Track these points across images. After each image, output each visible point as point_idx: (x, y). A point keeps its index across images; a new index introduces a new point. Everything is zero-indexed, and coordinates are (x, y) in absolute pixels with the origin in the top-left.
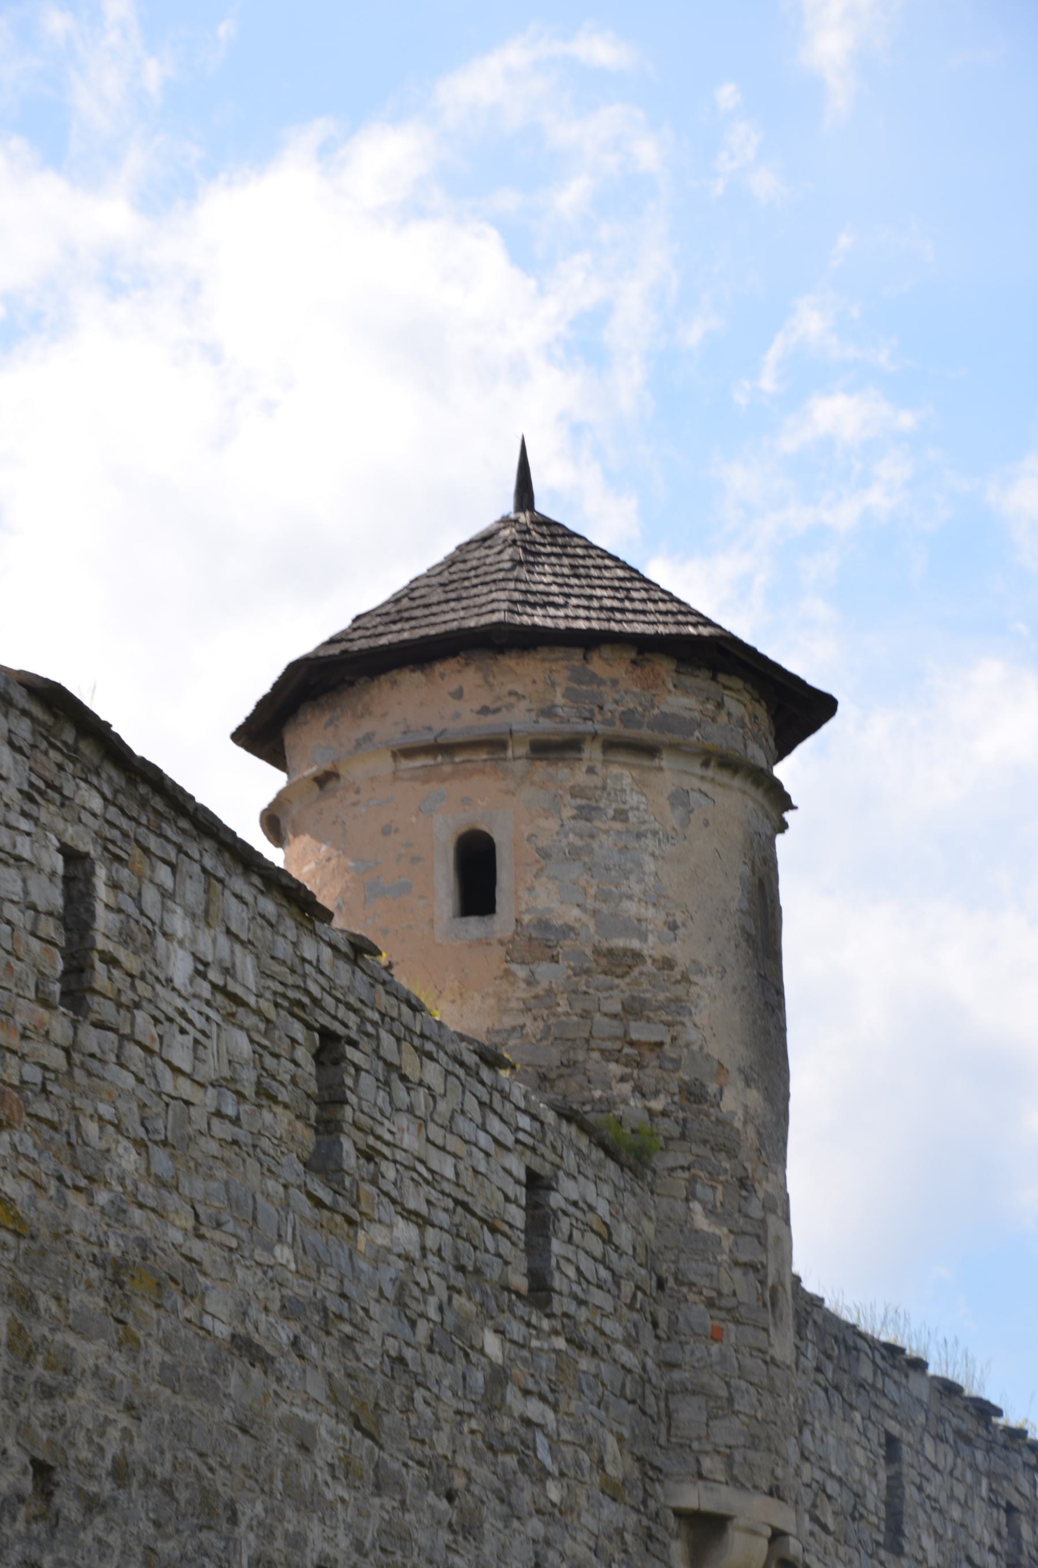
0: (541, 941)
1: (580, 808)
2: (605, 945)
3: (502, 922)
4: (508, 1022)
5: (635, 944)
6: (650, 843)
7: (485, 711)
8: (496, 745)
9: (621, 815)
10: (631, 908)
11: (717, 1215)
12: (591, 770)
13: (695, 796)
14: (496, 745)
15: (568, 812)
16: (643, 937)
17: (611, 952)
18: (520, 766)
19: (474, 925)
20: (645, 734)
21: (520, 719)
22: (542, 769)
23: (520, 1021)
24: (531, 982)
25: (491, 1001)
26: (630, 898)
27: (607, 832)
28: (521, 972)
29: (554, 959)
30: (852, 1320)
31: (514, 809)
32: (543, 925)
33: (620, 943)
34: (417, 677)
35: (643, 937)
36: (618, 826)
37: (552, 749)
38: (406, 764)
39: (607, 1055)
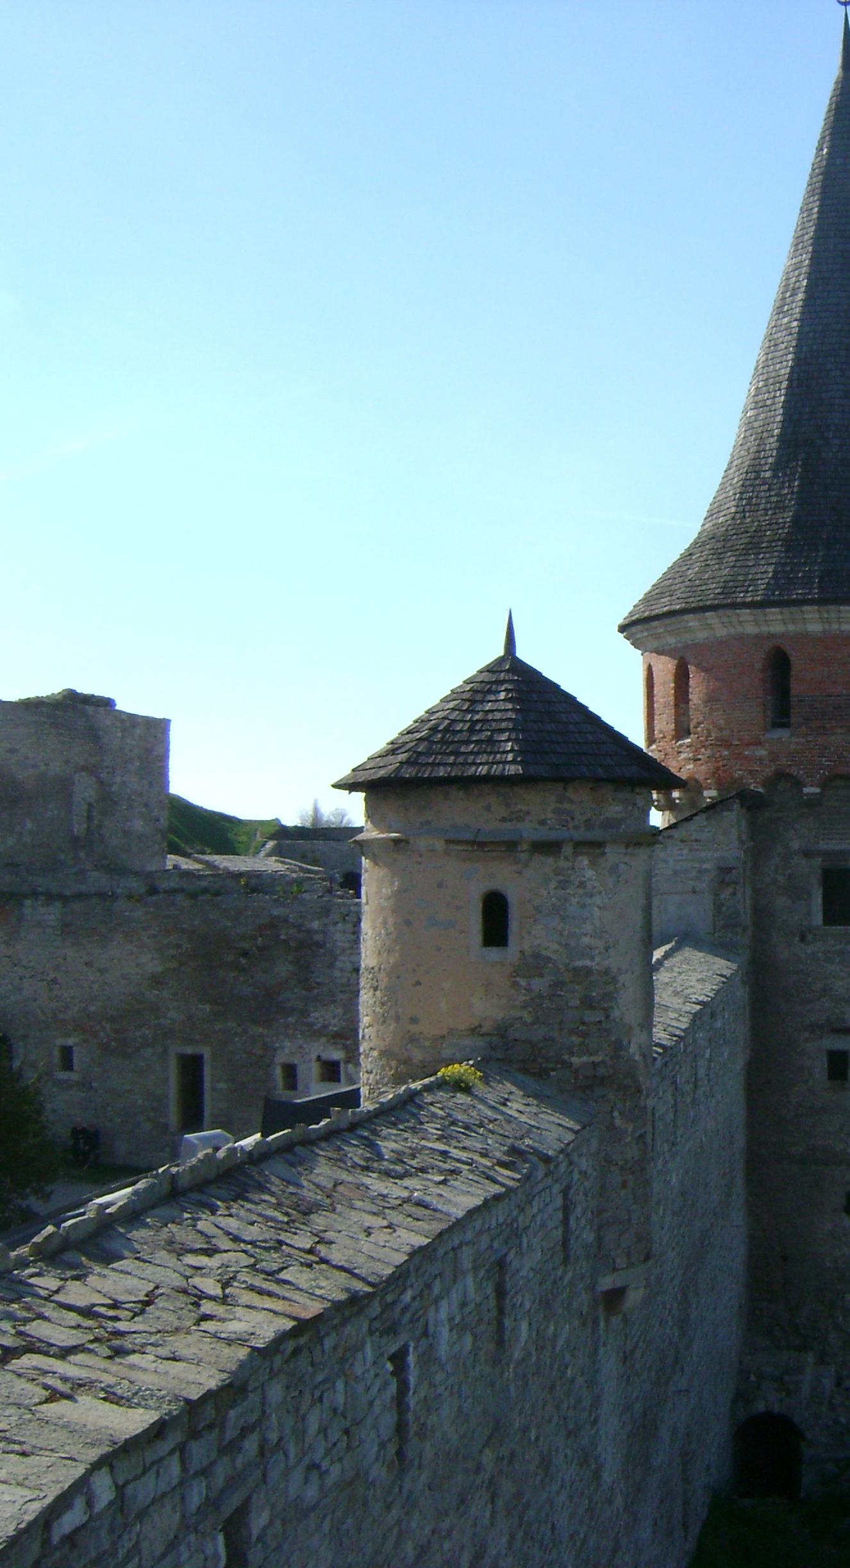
0: (534, 964)
1: (560, 882)
2: (573, 964)
3: (511, 953)
4: (515, 1013)
5: (588, 963)
6: (597, 900)
7: (504, 820)
8: (511, 846)
9: (582, 885)
10: (586, 940)
11: (405, 1103)
12: (566, 859)
13: (622, 866)
14: (511, 846)
15: (553, 885)
16: (592, 958)
17: (574, 969)
18: (523, 856)
19: (494, 954)
20: (596, 834)
21: (529, 830)
22: (538, 858)
23: (519, 1014)
24: (529, 990)
25: (504, 1001)
26: (585, 935)
27: (574, 895)
28: (523, 983)
29: (541, 975)
30: (516, 789)
31: (522, 884)
32: (536, 956)
33: (580, 963)
34: (461, 794)
35: (592, 958)
36: (581, 891)
37: (547, 847)
38: (452, 847)
39: (572, 1032)
